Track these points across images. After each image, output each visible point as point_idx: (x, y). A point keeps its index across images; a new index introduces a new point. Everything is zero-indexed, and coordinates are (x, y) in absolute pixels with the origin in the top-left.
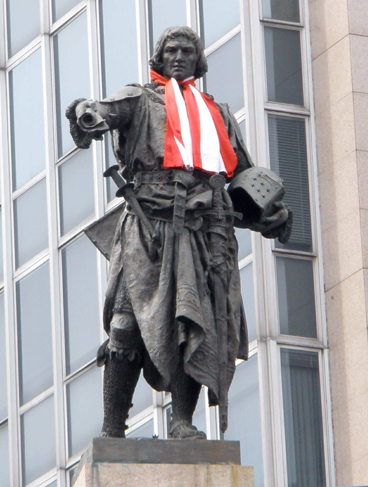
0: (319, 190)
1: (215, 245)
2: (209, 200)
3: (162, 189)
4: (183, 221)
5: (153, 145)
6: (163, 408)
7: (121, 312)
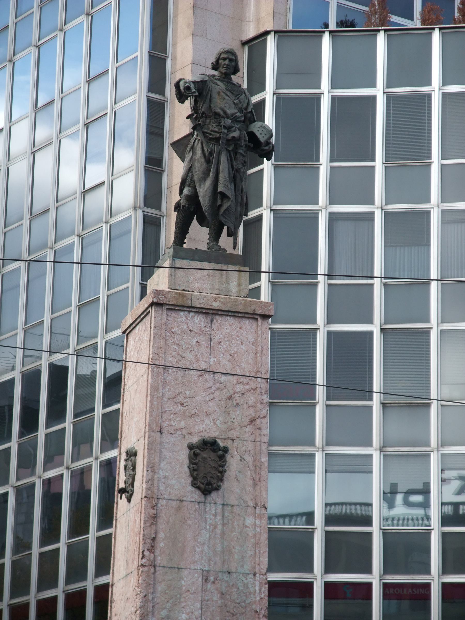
5: (212, 105)
6: (80, 237)
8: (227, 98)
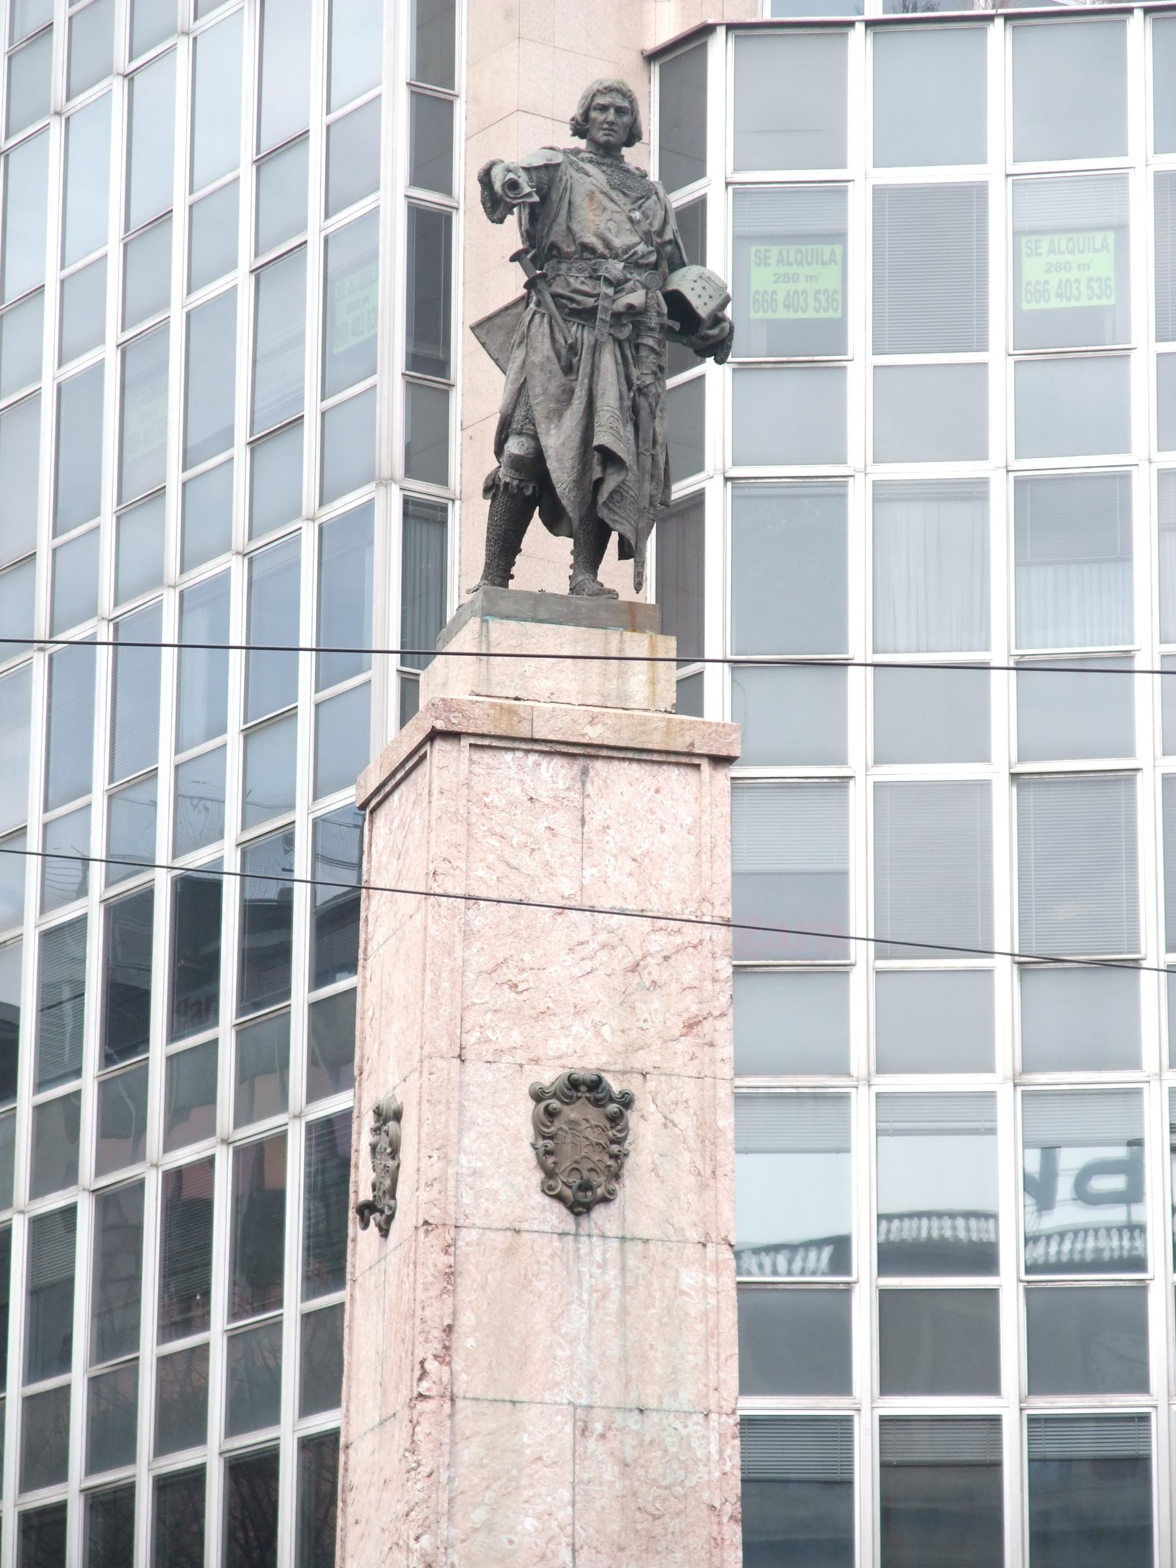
0: (463, 304)
3: (583, 283)
4: (608, 326)
5: (576, 227)
6: (245, 555)
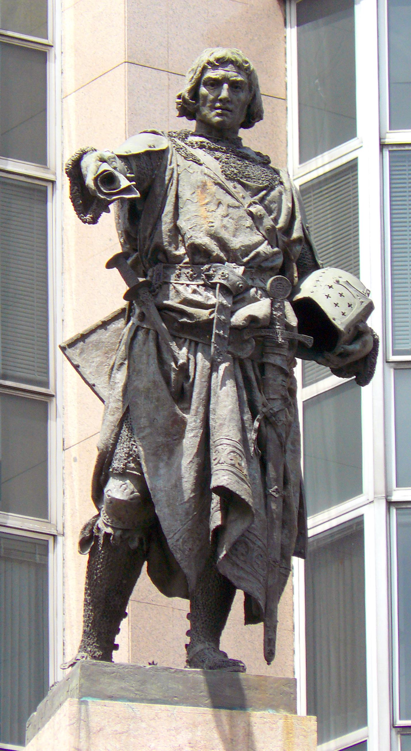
1: (271, 382)
2: (267, 314)
3: (194, 292)
4: (226, 343)
7: (123, 475)
8: (228, 199)
